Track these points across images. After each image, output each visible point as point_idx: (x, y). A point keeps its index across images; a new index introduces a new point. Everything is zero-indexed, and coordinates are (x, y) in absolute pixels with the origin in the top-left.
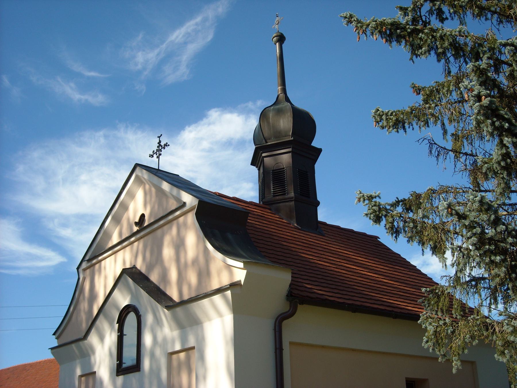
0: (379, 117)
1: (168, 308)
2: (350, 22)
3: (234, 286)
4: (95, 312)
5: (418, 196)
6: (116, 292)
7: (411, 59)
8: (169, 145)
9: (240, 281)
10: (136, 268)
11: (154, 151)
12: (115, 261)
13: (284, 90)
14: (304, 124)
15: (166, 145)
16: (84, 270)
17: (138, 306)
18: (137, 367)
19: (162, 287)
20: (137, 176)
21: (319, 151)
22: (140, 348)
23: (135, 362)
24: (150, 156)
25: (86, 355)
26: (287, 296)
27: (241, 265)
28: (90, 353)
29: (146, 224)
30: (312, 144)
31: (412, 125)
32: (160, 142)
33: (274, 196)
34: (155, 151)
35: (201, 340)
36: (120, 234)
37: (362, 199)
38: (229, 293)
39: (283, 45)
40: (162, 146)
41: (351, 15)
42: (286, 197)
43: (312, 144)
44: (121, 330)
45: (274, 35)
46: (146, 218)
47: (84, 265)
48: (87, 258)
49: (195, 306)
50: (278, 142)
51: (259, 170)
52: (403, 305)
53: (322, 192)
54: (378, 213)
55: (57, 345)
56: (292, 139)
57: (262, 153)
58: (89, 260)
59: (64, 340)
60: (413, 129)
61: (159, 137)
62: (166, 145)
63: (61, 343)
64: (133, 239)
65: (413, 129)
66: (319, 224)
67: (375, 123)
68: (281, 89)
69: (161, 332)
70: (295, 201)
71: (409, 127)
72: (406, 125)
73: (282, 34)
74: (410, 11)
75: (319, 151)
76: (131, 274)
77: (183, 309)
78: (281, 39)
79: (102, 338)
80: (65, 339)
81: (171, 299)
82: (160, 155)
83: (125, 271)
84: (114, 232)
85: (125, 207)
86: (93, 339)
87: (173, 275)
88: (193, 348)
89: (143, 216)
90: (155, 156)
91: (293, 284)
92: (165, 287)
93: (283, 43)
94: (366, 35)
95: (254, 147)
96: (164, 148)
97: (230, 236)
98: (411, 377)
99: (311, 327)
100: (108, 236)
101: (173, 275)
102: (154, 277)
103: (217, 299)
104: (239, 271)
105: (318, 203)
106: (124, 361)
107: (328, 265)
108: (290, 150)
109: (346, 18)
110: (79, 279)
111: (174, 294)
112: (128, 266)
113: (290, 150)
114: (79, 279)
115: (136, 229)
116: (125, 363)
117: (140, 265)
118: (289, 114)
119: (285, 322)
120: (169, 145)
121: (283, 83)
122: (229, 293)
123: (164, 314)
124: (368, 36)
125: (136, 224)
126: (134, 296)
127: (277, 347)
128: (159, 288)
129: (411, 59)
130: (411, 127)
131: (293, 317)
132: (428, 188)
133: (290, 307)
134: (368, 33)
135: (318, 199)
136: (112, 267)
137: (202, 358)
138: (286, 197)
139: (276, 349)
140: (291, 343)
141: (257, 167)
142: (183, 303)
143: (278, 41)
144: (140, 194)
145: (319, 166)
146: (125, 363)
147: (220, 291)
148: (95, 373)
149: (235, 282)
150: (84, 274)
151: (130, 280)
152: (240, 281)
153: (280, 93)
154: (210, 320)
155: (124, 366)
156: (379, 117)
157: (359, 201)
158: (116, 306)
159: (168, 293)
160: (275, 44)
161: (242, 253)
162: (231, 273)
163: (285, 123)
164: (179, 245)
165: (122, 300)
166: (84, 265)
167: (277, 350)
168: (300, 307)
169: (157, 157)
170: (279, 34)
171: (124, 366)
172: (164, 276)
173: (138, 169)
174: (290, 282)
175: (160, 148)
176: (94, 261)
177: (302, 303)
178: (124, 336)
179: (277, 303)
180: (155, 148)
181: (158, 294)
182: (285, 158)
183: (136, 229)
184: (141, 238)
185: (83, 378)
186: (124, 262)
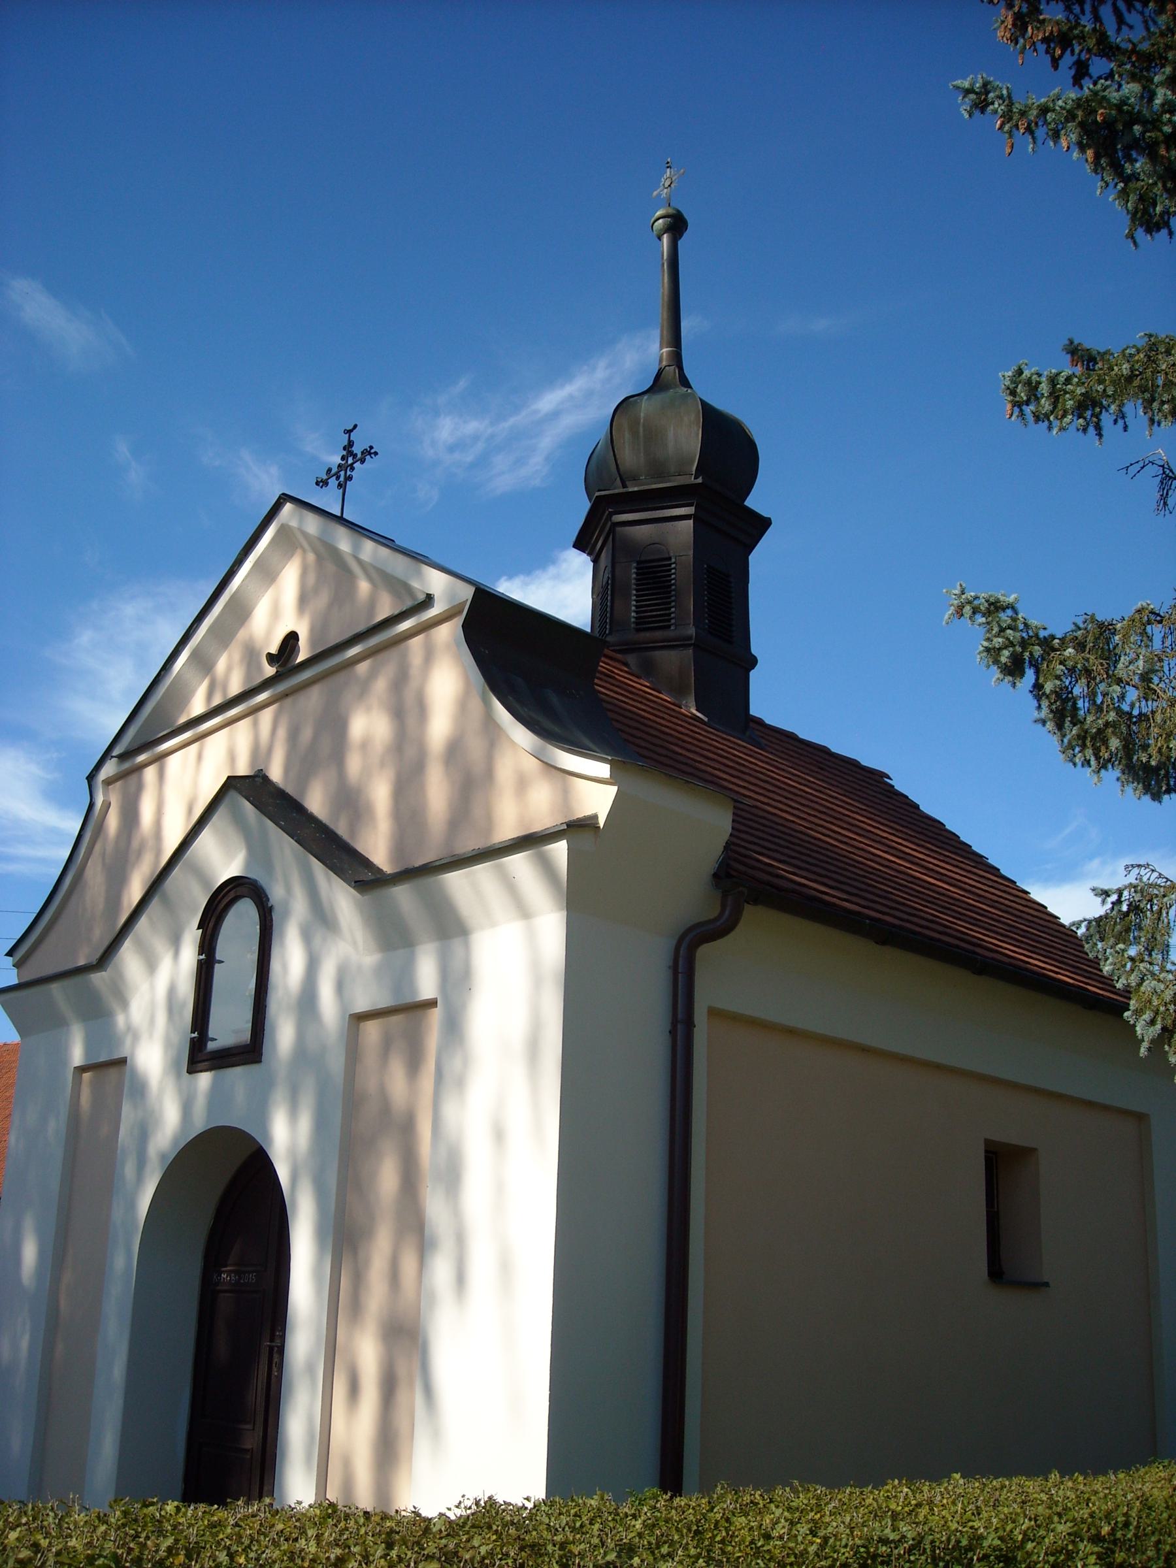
0: (1024, 393)
1: (361, 886)
2: (981, 105)
4: (135, 891)
5: (1105, 630)
6: (206, 838)
7: (1131, 236)
8: (376, 453)
9: (595, 817)
10: (266, 779)
11: (329, 470)
12: (200, 757)
13: (677, 358)
14: (729, 452)
15: (370, 454)
16: (108, 782)
17: (263, 881)
18: (251, 1051)
19: (342, 830)
20: (283, 530)
21: (765, 523)
23: (246, 1036)
24: (317, 483)
25: (98, 1013)
26: (716, 876)
27: (602, 769)
28: (115, 1006)
29: (301, 657)
30: (746, 503)
31: (1123, 417)
32: (351, 444)
33: (638, 630)
35: (458, 980)
36: (210, 695)
37: (967, 610)
38: (560, 850)
39: (680, 243)
40: (356, 455)
41: (985, 84)
42: (671, 633)
43: (746, 503)
44: (207, 947)
45: (659, 213)
46: (303, 642)
48: (117, 751)
49: (456, 881)
51: (595, 561)
52: (1008, 949)
53: (763, 635)
54: (1018, 649)
55: (16, 981)
56: (700, 480)
57: (611, 514)
58: (123, 757)
59: (35, 970)
60: (1125, 428)
61: (349, 432)
62: (369, 452)
63: (26, 979)
64: (262, 697)
65: (1125, 428)
66: (752, 724)
67: (1009, 406)
68: (669, 353)
69: (325, 960)
70: (698, 646)
71: (1115, 422)
72: (1106, 419)
73: (678, 211)
74: (1161, 84)
75: (765, 523)
76: (249, 789)
77: (407, 887)
78: (677, 225)
79: (151, 966)
80: (41, 966)
81: (366, 863)
82: (350, 478)
83: (232, 784)
84: (193, 692)
85: (240, 612)
86: (129, 958)
87: (381, 794)
88: (432, 1003)
89: (291, 639)
90: (333, 482)
91: (734, 844)
92: (353, 829)
93: (681, 235)
94: (1034, 138)
95: (585, 505)
96: (363, 461)
97: (554, 699)
99: (770, 973)
100: (181, 696)
101: (381, 794)
102: (316, 802)
103: (519, 863)
104: (593, 786)
105: (753, 662)
106: (211, 1034)
107: (792, 818)
108: (689, 510)
109: (968, 92)
110: (91, 805)
111: (378, 847)
113: (689, 510)
114: (91, 805)
115: (270, 671)
116: (213, 1040)
118: (693, 417)
119: (704, 951)
120: (376, 453)
121: (675, 337)
122: (560, 850)
123: (343, 900)
124: (1040, 142)
125: (271, 658)
126: (258, 851)
127: (680, 1016)
128: (335, 834)
129: (1131, 236)
130: (1121, 422)
131: (732, 934)
132: (1139, 606)
133: (723, 906)
134: (1041, 132)
135: (754, 651)
136: (188, 778)
137: (454, 1028)
138: (671, 633)
139: (674, 1023)
140: (713, 1012)
141: (589, 554)
142: (408, 874)
143: (669, 229)
144: (290, 577)
146: (213, 1040)
147: (529, 841)
148: (123, 1061)
149: (579, 820)
150: (105, 794)
151: (247, 806)
152: (595, 817)
153: (664, 363)
154: (493, 924)
155: (211, 1046)
156: (1024, 393)
157: (959, 611)
158: (201, 875)
159: (360, 847)
160: (660, 238)
161: (591, 745)
162: (565, 795)
163: (685, 439)
164: (407, 711)
165: (221, 858)
166: (110, 769)
167: (679, 1026)
168: (751, 913)
169: (340, 485)
170: (671, 211)
171: (211, 1046)
172: (350, 800)
173: (288, 507)
174: (726, 837)
175: (350, 461)
176: (141, 758)
177: (755, 901)
178: (217, 965)
179: (686, 892)
181: (335, 851)
182: (678, 531)
183: (270, 671)
184: (286, 695)
185: (87, 1076)
186: (232, 758)
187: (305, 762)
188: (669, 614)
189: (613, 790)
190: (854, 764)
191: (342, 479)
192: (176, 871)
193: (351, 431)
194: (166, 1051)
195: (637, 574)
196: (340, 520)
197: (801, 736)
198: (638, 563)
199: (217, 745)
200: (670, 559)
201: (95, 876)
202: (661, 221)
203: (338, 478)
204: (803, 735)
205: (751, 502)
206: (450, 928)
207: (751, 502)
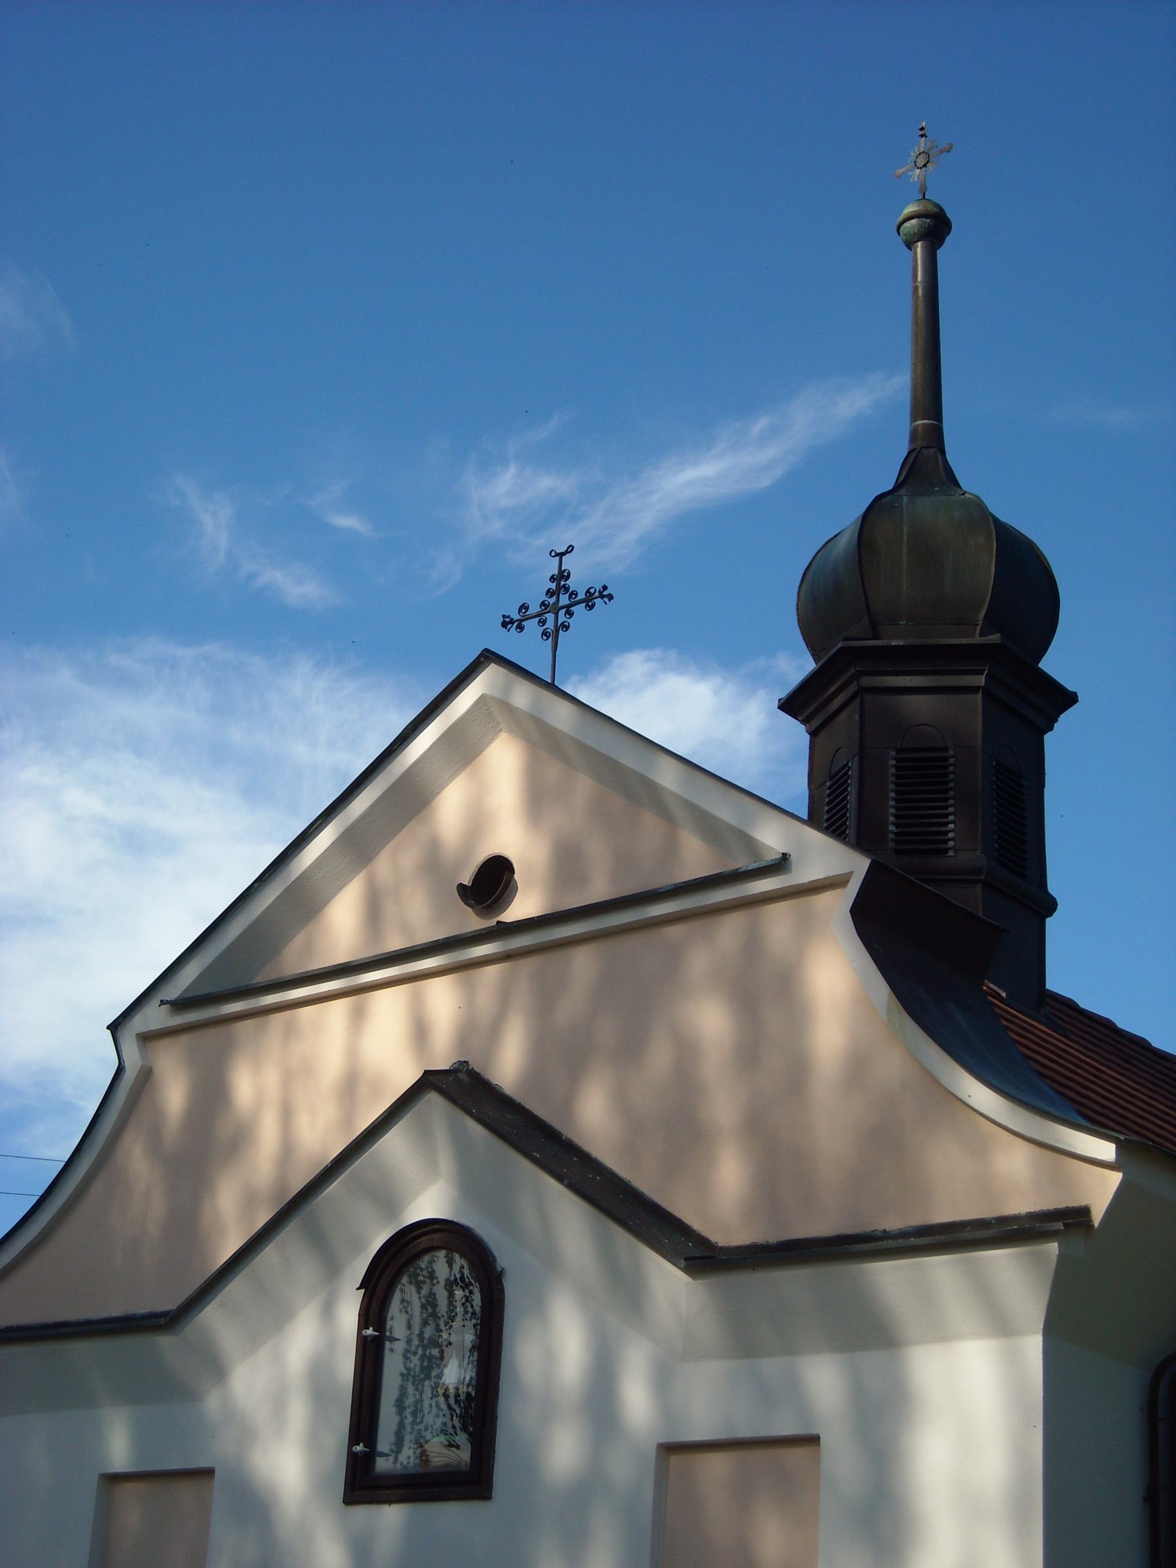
3: (1073, 1219)
8: (610, 597)
11: (524, 607)
14: (1025, 592)
15: (602, 596)
16: (147, 1038)
21: (1069, 699)
22: (88, 1322)
27: (1106, 1150)
30: (1041, 665)
34: (534, 609)
39: (940, 253)
43: (1041, 665)
47: (155, 1017)
48: (174, 991)
49: (889, 1277)
50: (963, 641)
56: (995, 638)
73: (941, 209)
75: (1069, 699)
76: (459, 1087)
78: (935, 228)
83: (429, 1082)
90: (531, 625)
93: (941, 242)
98: (223, 1293)
102: (594, 1117)
103: (1001, 1261)
112: (442, 1063)
113: (981, 680)
114: (120, 1070)
117: (508, 1067)
120: (610, 597)
126: (469, 1184)
141: (805, 722)
145: (1062, 744)
158: (387, 1199)
180: (535, 592)
187: (562, 1054)
188: (947, 833)
189: (1116, 1178)
190: (1106, 1025)
191: (550, 624)
192: (334, 1187)
193: (561, 555)
194: (443, 1466)
195: (897, 768)
196: (552, 687)
197: (1120, 1025)
198: (898, 751)
199: (388, 1009)
200: (946, 749)
201: (137, 1161)
202: (914, 221)
203: (543, 622)
204: (1085, 1003)
205: (1049, 664)
206: (871, 1336)
207: (1049, 664)
